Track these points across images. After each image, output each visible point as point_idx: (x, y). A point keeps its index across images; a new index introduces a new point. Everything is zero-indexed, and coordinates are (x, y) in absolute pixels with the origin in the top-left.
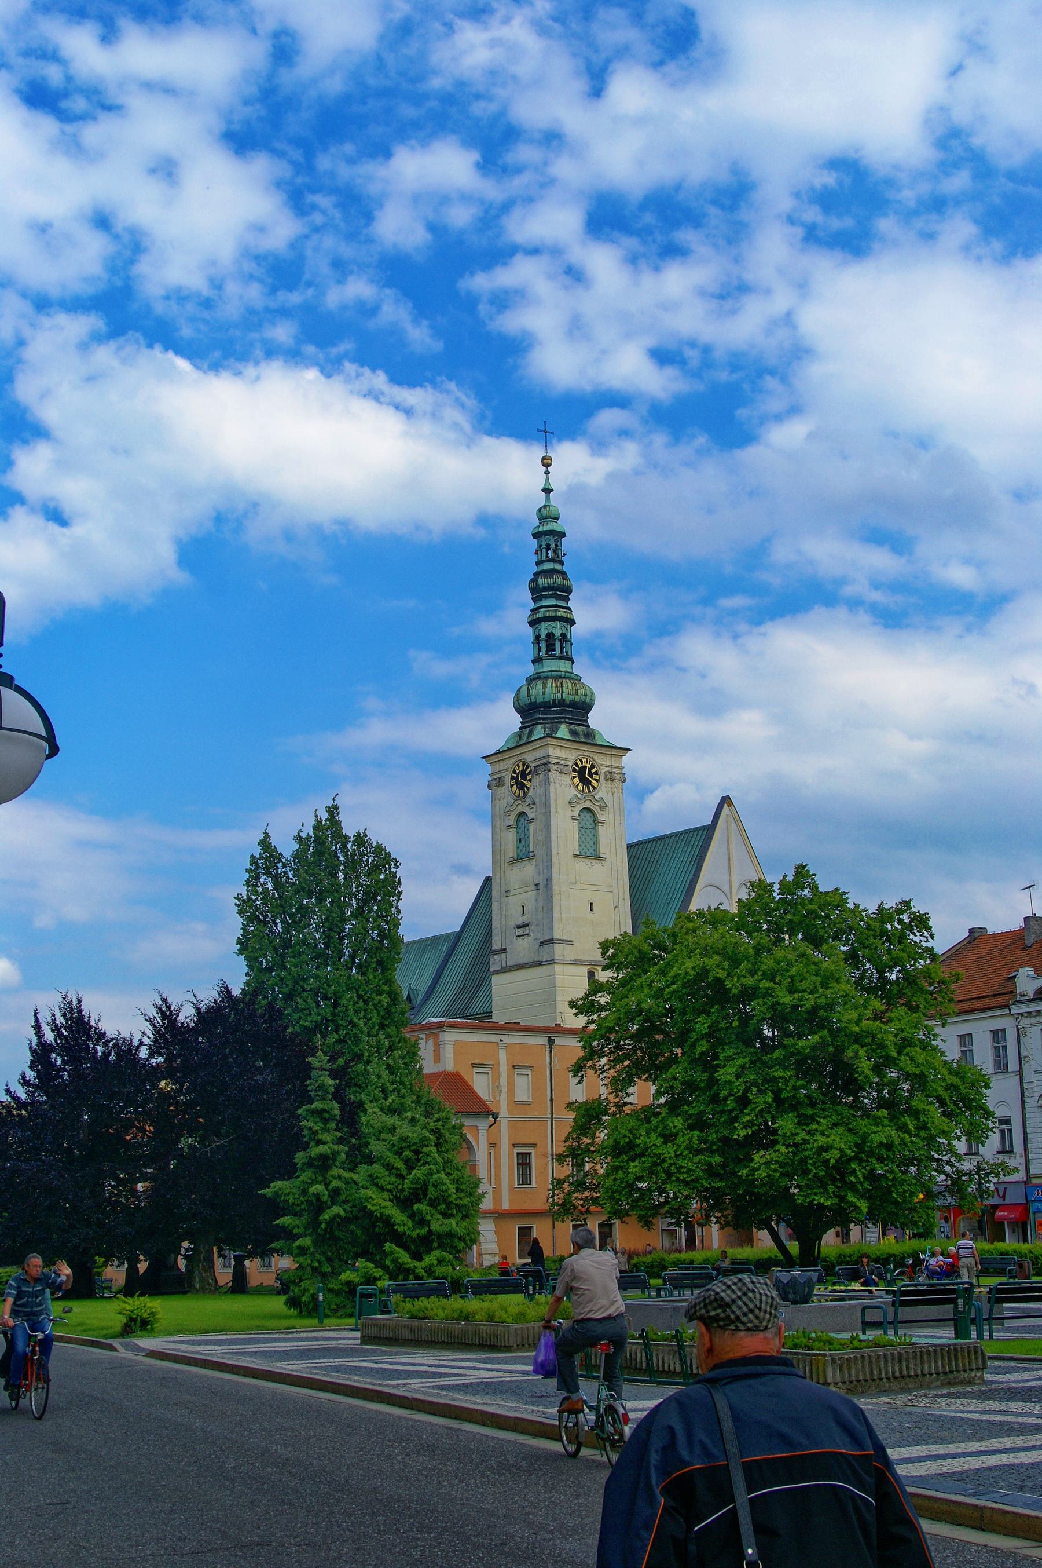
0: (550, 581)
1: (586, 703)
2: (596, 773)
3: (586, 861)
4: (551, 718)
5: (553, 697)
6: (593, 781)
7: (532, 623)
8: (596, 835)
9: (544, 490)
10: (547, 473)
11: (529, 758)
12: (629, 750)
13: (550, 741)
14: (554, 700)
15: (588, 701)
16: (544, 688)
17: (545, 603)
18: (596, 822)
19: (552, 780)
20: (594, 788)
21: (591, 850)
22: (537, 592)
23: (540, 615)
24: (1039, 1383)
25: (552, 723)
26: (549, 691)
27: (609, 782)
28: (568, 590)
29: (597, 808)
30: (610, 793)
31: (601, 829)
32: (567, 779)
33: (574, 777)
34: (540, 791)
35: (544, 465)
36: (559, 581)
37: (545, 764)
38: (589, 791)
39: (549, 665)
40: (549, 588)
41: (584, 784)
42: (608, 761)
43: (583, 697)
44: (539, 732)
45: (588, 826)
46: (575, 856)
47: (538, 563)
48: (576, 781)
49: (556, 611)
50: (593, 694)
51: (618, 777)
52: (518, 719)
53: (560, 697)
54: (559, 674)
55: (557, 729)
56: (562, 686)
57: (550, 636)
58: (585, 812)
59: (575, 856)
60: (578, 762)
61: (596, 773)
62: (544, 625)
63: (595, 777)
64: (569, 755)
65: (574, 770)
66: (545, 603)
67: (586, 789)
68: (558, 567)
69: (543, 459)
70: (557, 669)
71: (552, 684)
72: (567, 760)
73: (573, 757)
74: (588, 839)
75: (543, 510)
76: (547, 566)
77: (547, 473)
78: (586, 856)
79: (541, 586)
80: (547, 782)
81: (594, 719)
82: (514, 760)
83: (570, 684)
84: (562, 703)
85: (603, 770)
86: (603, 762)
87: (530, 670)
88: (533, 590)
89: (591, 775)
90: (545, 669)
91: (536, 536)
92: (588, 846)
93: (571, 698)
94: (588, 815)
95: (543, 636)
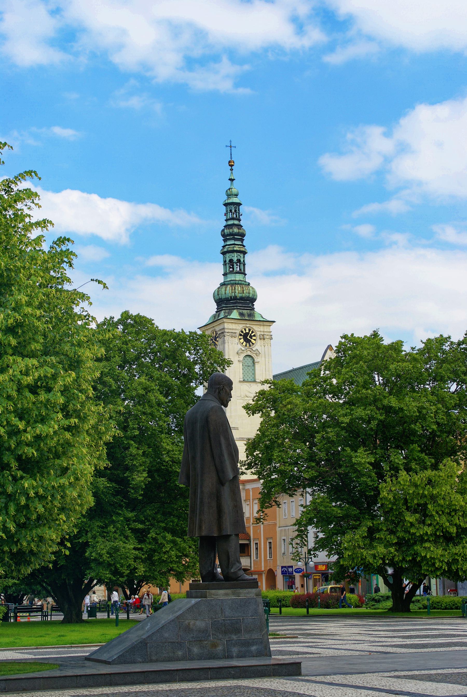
0: (231, 230)
1: (250, 298)
2: (254, 336)
3: (248, 384)
4: (230, 307)
5: (230, 295)
6: (252, 340)
7: (224, 253)
8: (254, 370)
9: (230, 179)
10: (232, 170)
11: (217, 329)
12: (274, 322)
13: (225, 320)
14: (231, 297)
15: (251, 296)
16: (225, 290)
17: (229, 243)
18: (254, 363)
19: (226, 341)
20: (253, 344)
21: (251, 378)
22: (225, 237)
23: (225, 250)
24: (465, 670)
25: (230, 309)
26: (228, 292)
27: (262, 340)
28: (243, 235)
29: (255, 355)
30: (263, 346)
31: (257, 366)
32: (236, 340)
33: (240, 339)
34: (221, 347)
35: (230, 165)
36: (236, 230)
37: (223, 333)
38: (250, 346)
39: (231, 277)
40: (231, 234)
41: (246, 342)
42: (262, 329)
43: (247, 294)
44: (222, 314)
45: (250, 365)
46: (240, 382)
47: (226, 220)
48: (242, 341)
49: (233, 247)
50: (254, 291)
51: (268, 337)
52: (214, 307)
53: (234, 295)
54: (235, 282)
55: (231, 313)
56: (235, 289)
57: (231, 261)
58: (248, 358)
59: (240, 382)
60: (243, 330)
61: (254, 336)
62: (228, 255)
63: (254, 338)
64: (238, 327)
65: (240, 335)
66: (229, 243)
67: (248, 345)
68: (236, 222)
69: (229, 162)
70: (235, 279)
71: (230, 288)
72: (236, 329)
73: (240, 328)
74: (249, 372)
75: (228, 191)
76: (230, 222)
77: (232, 170)
78: (248, 382)
79: (226, 234)
80: (224, 342)
81: (257, 305)
82: (211, 330)
83: (240, 288)
84: (235, 298)
85: (258, 334)
86: (258, 329)
87: (222, 279)
88: (223, 235)
89: (251, 337)
90: (228, 280)
91: (226, 205)
92: (249, 376)
93: (240, 295)
94: (249, 359)
95: (227, 261)
